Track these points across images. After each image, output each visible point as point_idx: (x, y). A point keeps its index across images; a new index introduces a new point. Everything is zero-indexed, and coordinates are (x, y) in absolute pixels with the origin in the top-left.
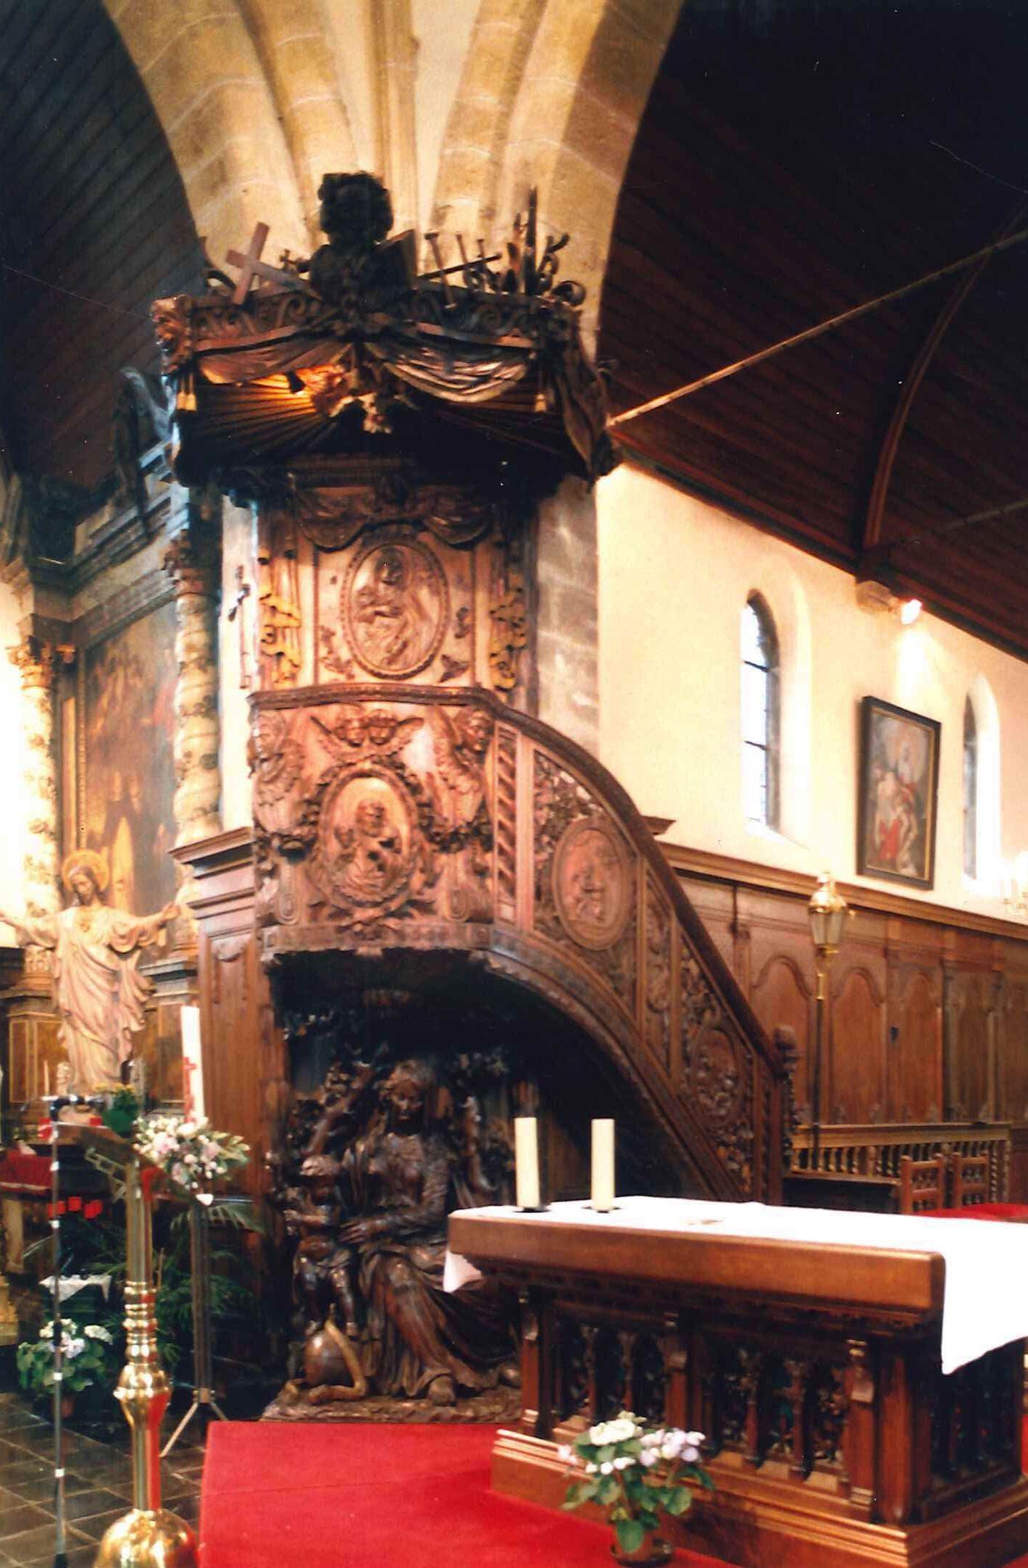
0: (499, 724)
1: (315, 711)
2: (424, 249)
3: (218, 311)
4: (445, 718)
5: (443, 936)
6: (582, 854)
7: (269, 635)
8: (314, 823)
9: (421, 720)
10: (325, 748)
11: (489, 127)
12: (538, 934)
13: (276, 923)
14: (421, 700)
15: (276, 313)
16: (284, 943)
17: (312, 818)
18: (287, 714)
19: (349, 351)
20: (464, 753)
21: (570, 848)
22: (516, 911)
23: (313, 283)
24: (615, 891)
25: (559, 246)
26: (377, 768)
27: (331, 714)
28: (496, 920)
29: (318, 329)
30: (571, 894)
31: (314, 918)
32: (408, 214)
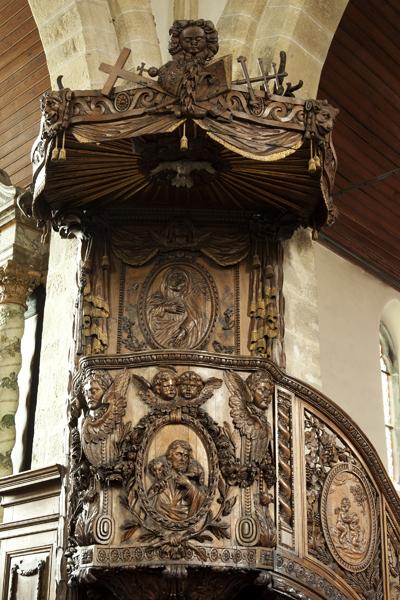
0: (277, 387)
1: (135, 372)
2: (236, 67)
3: (89, 99)
4: (239, 380)
5: (237, 557)
6: (344, 487)
7: (87, 322)
8: (134, 460)
9: (221, 381)
10: (144, 400)
11: (245, 28)
12: (311, 557)
13: (95, 543)
14: (210, 364)
15: (132, 101)
16: (99, 560)
17: (132, 456)
18: (113, 373)
19: (182, 126)
20: (250, 406)
21: (333, 487)
22: (294, 540)
23: (160, 83)
24: (364, 522)
25: (297, 88)
26: (188, 418)
27: (149, 374)
28: (278, 545)
29: (161, 111)
30: (334, 522)
31: (125, 539)
32: (230, 44)
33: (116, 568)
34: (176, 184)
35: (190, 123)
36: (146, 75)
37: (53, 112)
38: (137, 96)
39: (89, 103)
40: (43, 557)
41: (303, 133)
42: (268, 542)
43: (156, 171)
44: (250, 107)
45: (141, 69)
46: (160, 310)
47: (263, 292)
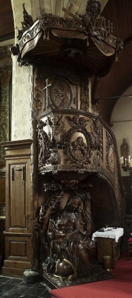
4: (93, 120)
23: (82, 21)
31: (65, 163)
33: (64, 171)
34: (70, 55)
35: (89, 37)
36: (78, 16)
37: (46, 22)
38: (74, 23)
39: (58, 21)
40: (24, 165)
41: (115, 49)
42: (99, 165)
43: (66, 50)
44: (105, 36)
45: (76, 14)
46: (56, 95)
47: (85, 94)
